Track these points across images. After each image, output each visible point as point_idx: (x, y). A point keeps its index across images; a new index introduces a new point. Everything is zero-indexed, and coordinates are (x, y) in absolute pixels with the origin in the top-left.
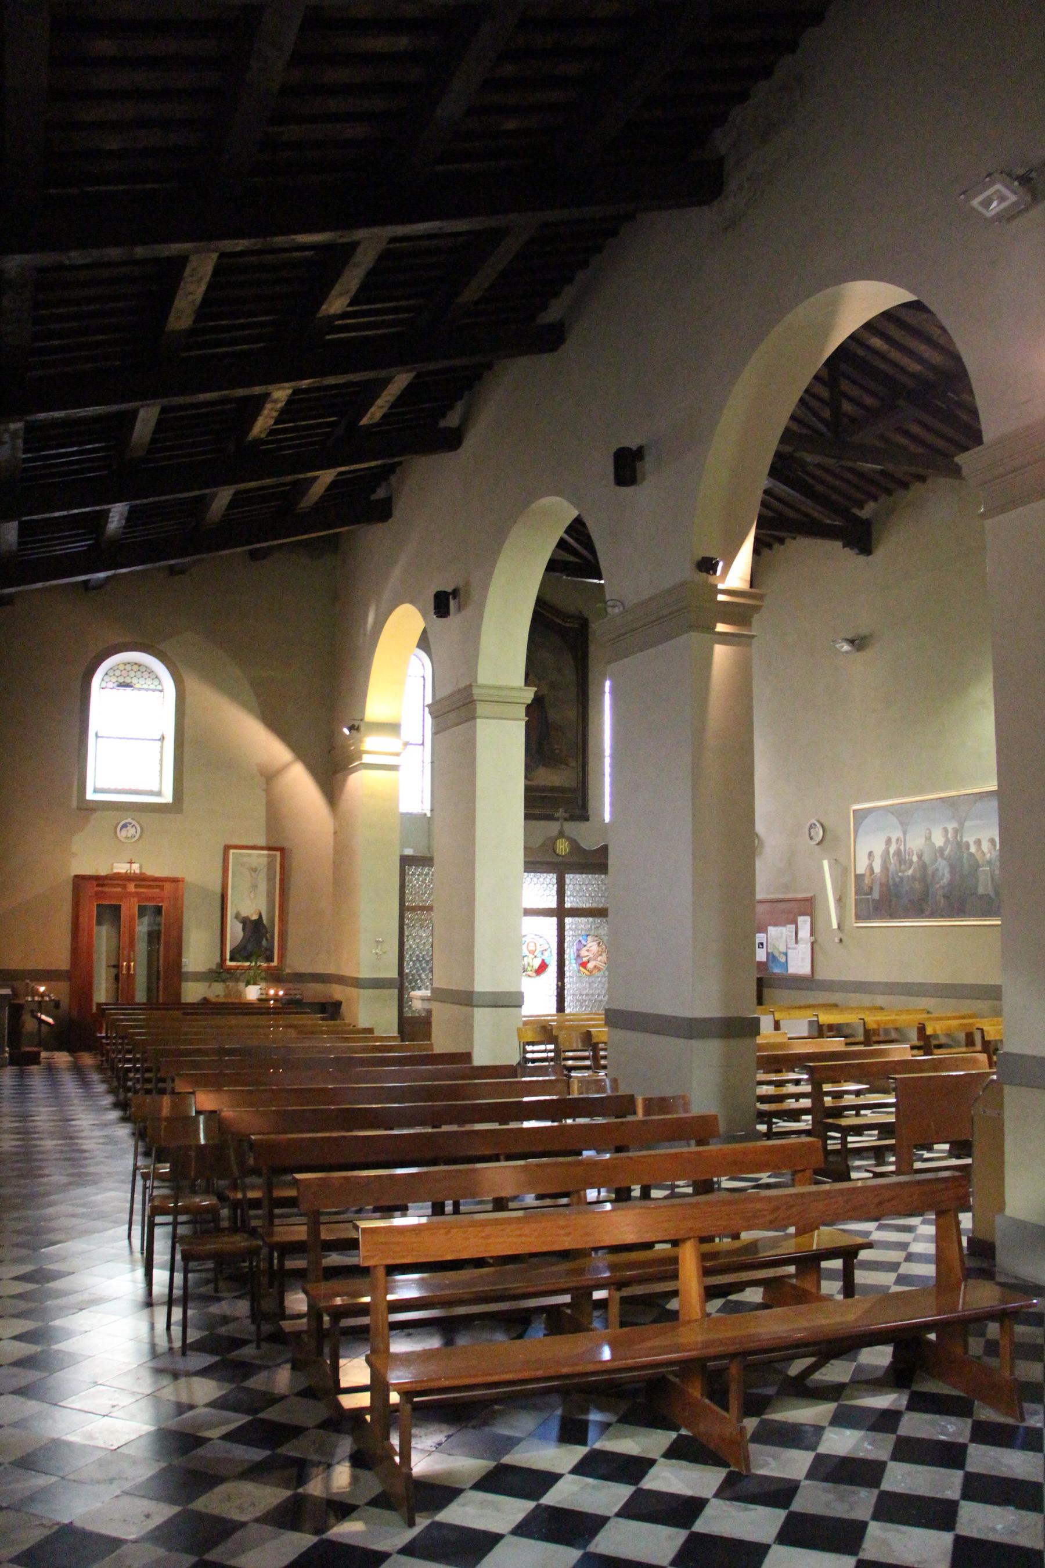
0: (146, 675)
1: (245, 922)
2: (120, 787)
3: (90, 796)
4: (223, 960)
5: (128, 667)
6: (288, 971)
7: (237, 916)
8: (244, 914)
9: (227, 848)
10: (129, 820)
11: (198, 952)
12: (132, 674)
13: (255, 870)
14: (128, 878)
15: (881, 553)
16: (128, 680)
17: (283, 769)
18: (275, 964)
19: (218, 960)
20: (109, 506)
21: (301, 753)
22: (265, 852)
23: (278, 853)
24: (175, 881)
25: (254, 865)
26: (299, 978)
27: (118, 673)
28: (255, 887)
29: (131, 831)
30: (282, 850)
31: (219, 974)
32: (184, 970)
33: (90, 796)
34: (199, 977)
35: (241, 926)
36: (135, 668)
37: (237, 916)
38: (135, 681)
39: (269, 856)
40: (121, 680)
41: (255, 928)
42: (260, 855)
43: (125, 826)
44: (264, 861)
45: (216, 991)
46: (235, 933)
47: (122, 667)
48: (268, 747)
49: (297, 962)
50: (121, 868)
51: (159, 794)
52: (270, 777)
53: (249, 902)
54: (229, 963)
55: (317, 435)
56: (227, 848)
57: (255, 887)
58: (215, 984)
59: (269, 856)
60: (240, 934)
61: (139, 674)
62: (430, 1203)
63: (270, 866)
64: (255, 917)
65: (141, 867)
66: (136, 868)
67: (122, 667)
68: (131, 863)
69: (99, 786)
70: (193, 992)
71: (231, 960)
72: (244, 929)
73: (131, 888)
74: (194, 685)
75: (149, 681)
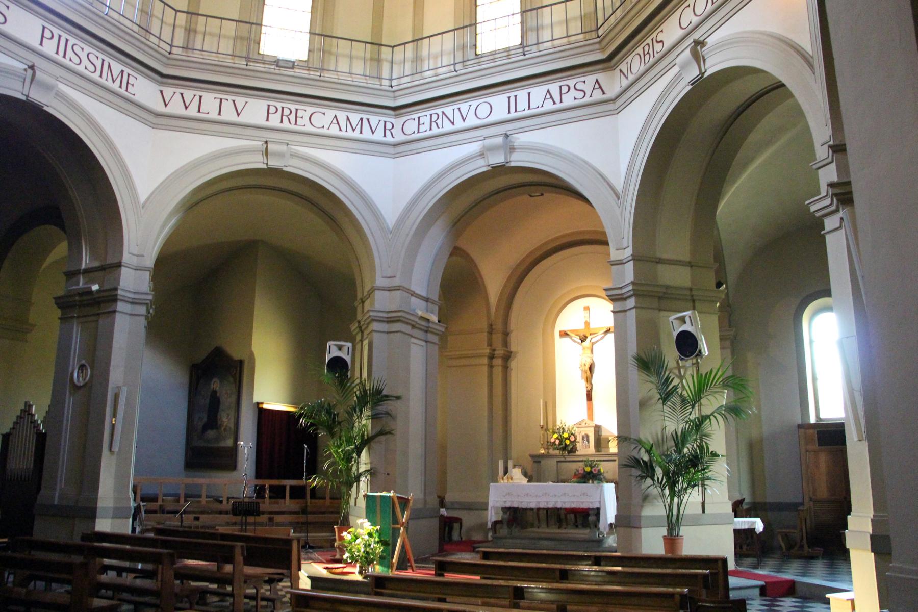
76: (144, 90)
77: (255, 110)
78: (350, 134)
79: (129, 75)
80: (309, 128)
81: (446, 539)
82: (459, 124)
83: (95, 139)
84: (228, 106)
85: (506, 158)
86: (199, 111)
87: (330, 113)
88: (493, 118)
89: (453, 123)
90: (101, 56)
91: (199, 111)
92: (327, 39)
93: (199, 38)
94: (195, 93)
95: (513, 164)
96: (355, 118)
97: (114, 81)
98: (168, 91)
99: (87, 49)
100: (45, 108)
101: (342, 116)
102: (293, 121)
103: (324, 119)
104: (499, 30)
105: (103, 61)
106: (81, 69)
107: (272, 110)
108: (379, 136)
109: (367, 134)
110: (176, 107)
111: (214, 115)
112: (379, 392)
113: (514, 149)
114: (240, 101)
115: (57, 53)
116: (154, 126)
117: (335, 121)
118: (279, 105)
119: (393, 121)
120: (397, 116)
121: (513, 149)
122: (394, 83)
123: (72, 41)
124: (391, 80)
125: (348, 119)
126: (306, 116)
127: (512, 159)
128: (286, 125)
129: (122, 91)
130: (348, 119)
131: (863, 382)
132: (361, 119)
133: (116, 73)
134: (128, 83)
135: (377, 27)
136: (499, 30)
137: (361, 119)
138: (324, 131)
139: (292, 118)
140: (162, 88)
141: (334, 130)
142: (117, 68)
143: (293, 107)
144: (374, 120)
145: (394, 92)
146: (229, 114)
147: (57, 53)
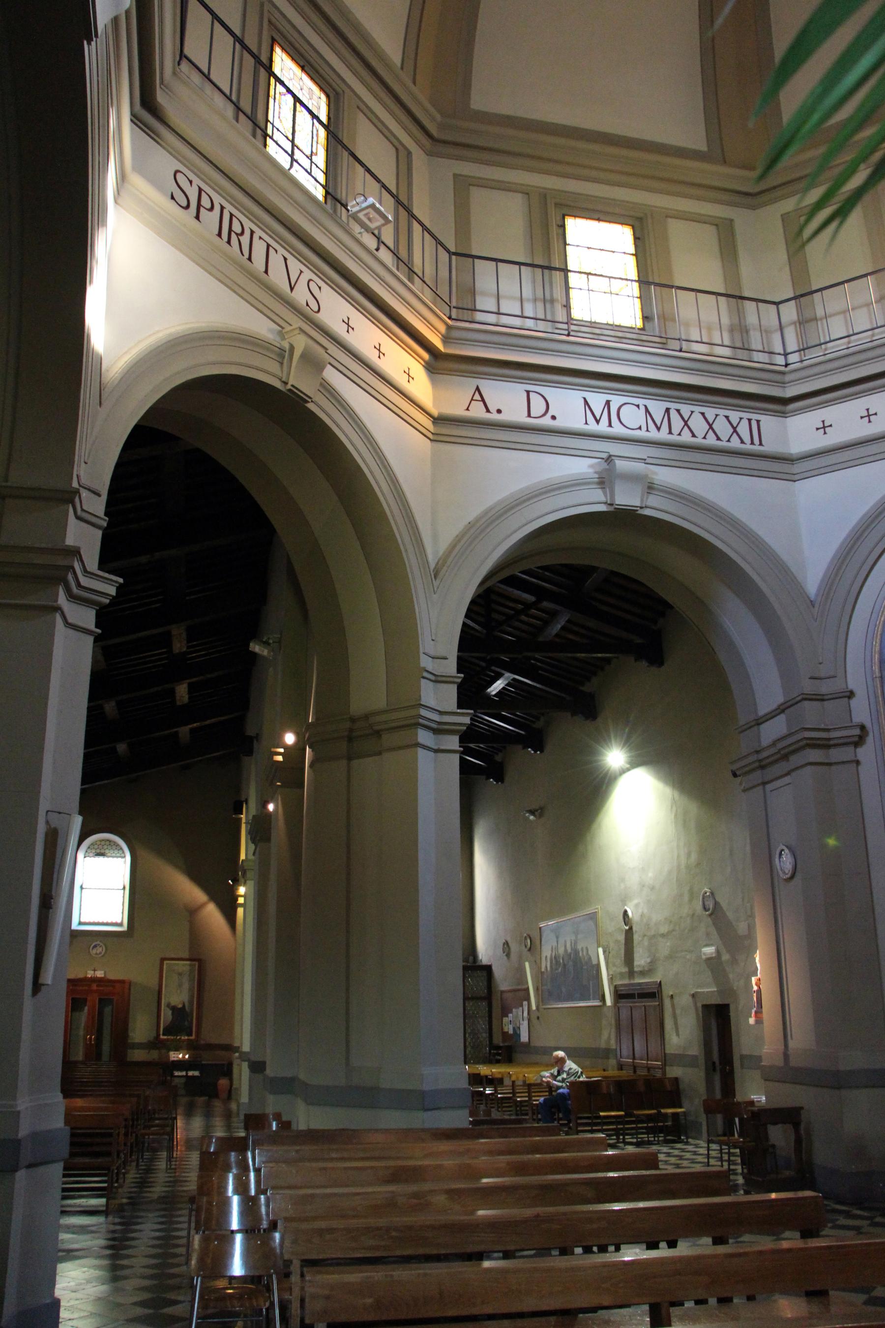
0: (114, 847)
1: (174, 1009)
2: (96, 921)
3: (75, 926)
4: (158, 1035)
5: (103, 843)
6: (202, 1042)
7: (168, 1005)
8: (173, 1004)
9: (163, 960)
10: (98, 942)
11: (141, 1029)
12: (105, 847)
13: (180, 974)
14: (94, 980)
15: (548, 748)
16: (102, 851)
17: (203, 905)
18: (193, 1037)
19: (154, 1034)
20: (503, 672)
21: (213, 897)
22: (188, 962)
23: (197, 963)
24: (122, 982)
25: (180, 971)
26: (210, 1047)
27: (96, 847)
28: (180, 985)
29: (99, 950)
30: (200, 961)
31: (155, 1044)
32: (129, 1041)
33: (75, 926)
34: (140, 1046)
35: (170, 1012)
36: (108, 843)
37: (168, 1005)
38: (107, 851)
39: (190, 965)
40: (98, 851)
41: (179, 1013)
42: (184, 965)
43: (95, 946)
44: (187, 968)
45: (154, 1055)
46: (166, 1016)
47: (98, 843)
48: (193, 893)
49: (210, 1036)
50: (90, 974)
51: (121, 925)
52: (193, 912)
53: (177, 995)
54: (162, 1037)
55: (515, 628)
56: (163, 960)
57: (180, 985)
58: (152, 1051)
59: (190, 965)
60: (170, 1017)
61: (109, 847)
62: (646, 1307)
63: (191, 971)
64: (180, 1006)
65: (105, 973)
66: (100, 974)
67: (98, 843)
68: (95, 970)
69: (82, 920)
70: (138, 1055)
71: (164, 1035)
72: (173, 1014)
73: (94, 987)
74: (142, 853)
75: (116, 852)
81: (579, 1121)
86: (529, 415)
91: (529, 415)
104: (240, 1324)
105: (750, 420)
112: (497, 772)
115: (758, 422)
117: (477, 397)
122: (793, 358)
123: (686, 409)
124: (786, 355)
125: (586, 402)
130: (586, 402)
131: (159, 233)
132: (668, 410)
133: (598, 408)
135: (830, 316)
136: (240, 1324)
137: (668, 410)
145: (779, 376)
147: (758, 422)
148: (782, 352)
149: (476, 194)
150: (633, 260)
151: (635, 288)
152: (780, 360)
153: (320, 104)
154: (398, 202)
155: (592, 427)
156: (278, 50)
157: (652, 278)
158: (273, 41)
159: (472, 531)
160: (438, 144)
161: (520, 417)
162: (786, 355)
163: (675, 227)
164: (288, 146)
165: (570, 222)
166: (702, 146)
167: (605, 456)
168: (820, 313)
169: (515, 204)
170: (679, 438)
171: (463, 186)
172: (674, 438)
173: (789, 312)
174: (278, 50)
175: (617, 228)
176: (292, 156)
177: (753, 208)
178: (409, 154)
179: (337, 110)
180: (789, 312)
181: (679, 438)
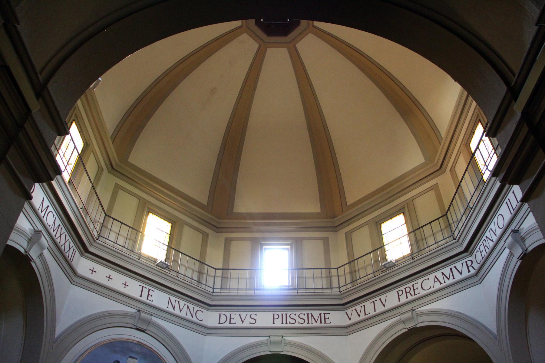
76: (337, 318)
77: (392, 299)
78: (448, 282)
79: (324, 314)
80: (423, 293)
82: (177, 312)
83: (377, 347)
84: (378, 303)
85: (522, 248)
86: (147, 299)
87: (432, 277)
88: (507, 221)
89: (181, 311)
90: (306, 313)
91: (147, 299)
92: (224, 271)
93: (324, 275)
94: (352, 309)
95: (530, 249)
96: (446, 271)
97: (316, 322)
98: (349, 311)
99: (298, 313)
100: (282, 353)
101: (439, 274)
102: (413, 294)
103: (429, 283)
106: (297, 325)
107: (276, 316)
108: (465, 274)
109: (458, 277)
110: (355, 318)
111: (373, 313)
113: (523, 238)
114: (383, 297)
116: (347, 334)
118: (403, 288)
119: (470, 258)
120: (471, 254)
121: (523, 239)
123: (289, 313)
126: (419, 286)
127: (527, 246)
128: (410, 298)
129: (323, 324)
134: (325, 318)
138: (432, 289)
139: (412, 292)
140: (346, 311)
141: (438, 286)
142: (316, 314)
143: (410, 285)
144: (458, 265)
145: (211, 295)
146: (380, 309)
148: (212, 287)
149: (121, 192)
150: (168, 237)
151: (166, 248)
152: (211, 290)
153: (80, 145)
154: (93, 186)
155: (170, 309)
156: (74, 124)
157: (173, 246)
158: (74, 120)
159: (366, 278)
160: (113, 169)
161: (137, 296)
162: (213, 289)
163: (186, 229)
164: (66, 164)
165: (150, 214)
166: (205, 203)
167: (138, 309)
168: (229, 276)
169: (134, 202)
170: (445, 284)
171: (117, 188)
172: (444, 285)
173: (219, 273)
174: (74, 124)
175: (166, 223)
176: (66, 167)
177: (217, 232)
178: (103, 170)
179: (86, 149)
180: (219, 273)
181: (445, 284)
